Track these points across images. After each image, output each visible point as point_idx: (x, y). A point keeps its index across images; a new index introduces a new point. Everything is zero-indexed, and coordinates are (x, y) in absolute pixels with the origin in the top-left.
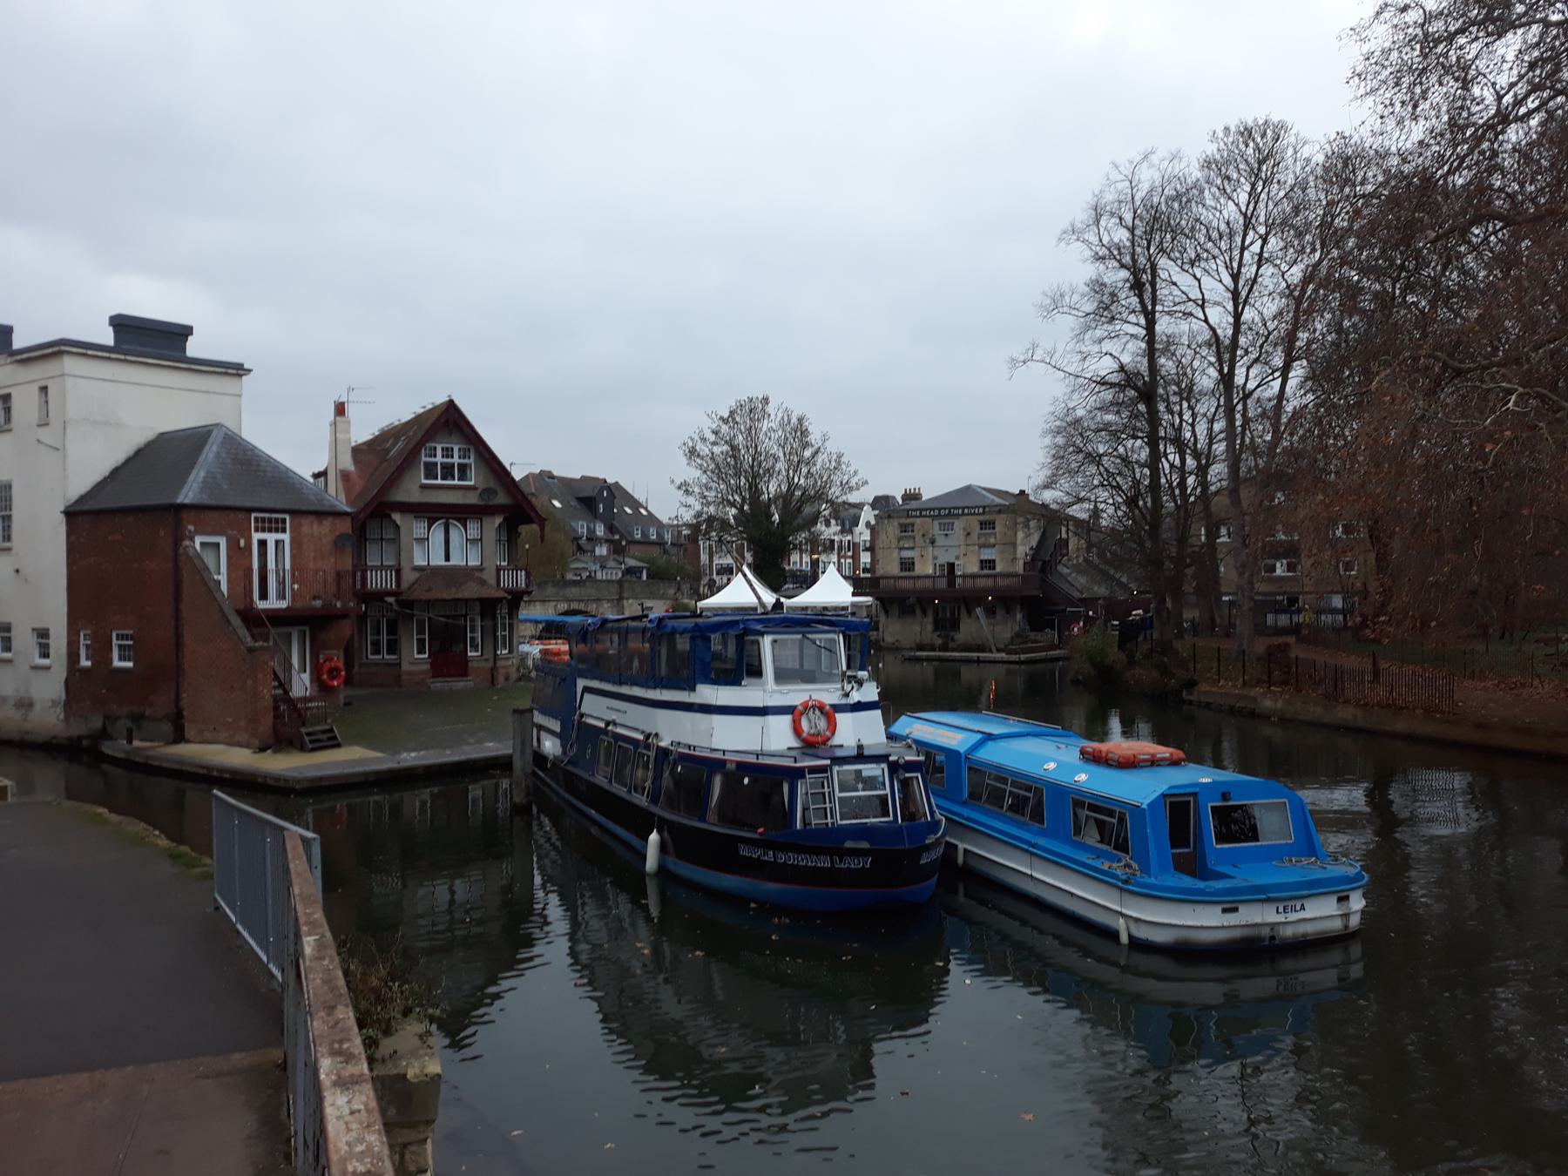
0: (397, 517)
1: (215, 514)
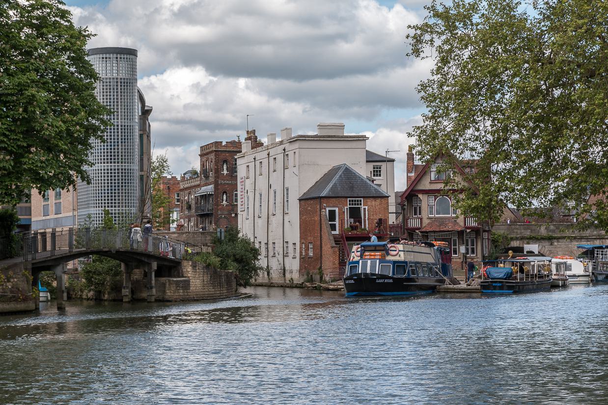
0: (420, 196)
1: (334, 199)
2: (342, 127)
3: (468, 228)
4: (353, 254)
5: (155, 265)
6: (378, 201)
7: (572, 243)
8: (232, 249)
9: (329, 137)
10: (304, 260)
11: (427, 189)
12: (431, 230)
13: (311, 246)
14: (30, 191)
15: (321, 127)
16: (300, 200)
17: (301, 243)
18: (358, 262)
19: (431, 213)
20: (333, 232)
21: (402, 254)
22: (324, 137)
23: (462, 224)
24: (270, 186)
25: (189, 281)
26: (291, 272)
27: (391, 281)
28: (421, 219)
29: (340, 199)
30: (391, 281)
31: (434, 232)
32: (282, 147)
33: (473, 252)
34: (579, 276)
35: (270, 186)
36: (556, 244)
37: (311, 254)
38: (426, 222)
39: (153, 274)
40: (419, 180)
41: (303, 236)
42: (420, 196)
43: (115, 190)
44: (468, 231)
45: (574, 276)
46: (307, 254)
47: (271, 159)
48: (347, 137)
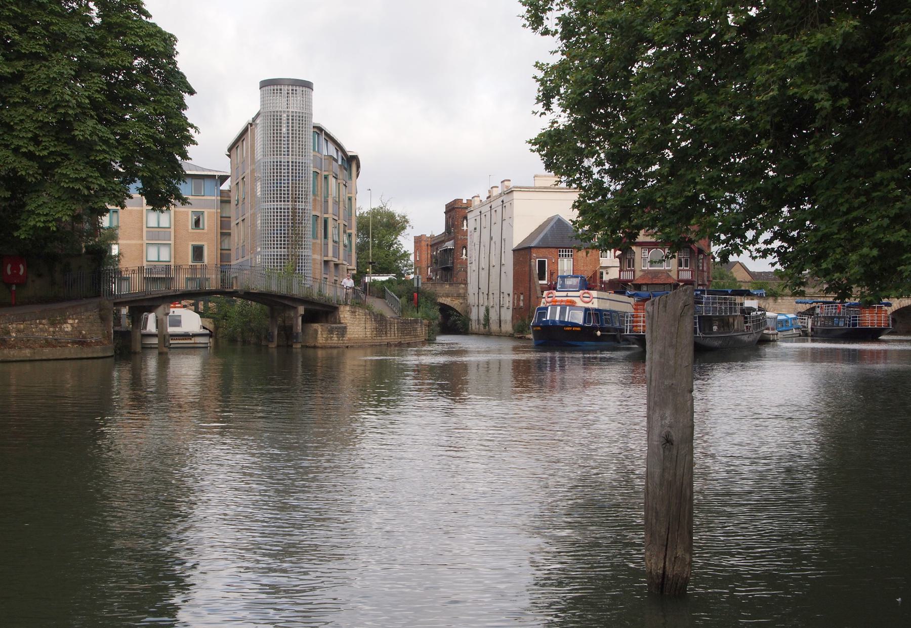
0: (634, 248)
1: (544, 250)
3: (682, 281)
4: (543, 300)
5: (301, 310)
9: (545, 188)
10: (516, 310)
12: (644, 282)
13: (522, 298)
16: (514, 251)
17: (514, 294)
18: (546, 308)
20: (541, 282)
21: (595, 301)
22: (540, 188)
23: (675, 277)
24: (491, 238)
25: (345, 328)
26: (506, 322)
27: (579, 329)
30: (579, 329)
31: (647, 285)
32: (501, 199)
34: (194, 335)
35: (491, 238)
37: (522, 304)
38: (638, 274)
39: (300, 318)
41: (516, 287)
45: (186, 336)
46: (518, 304)
47: (493, 211)
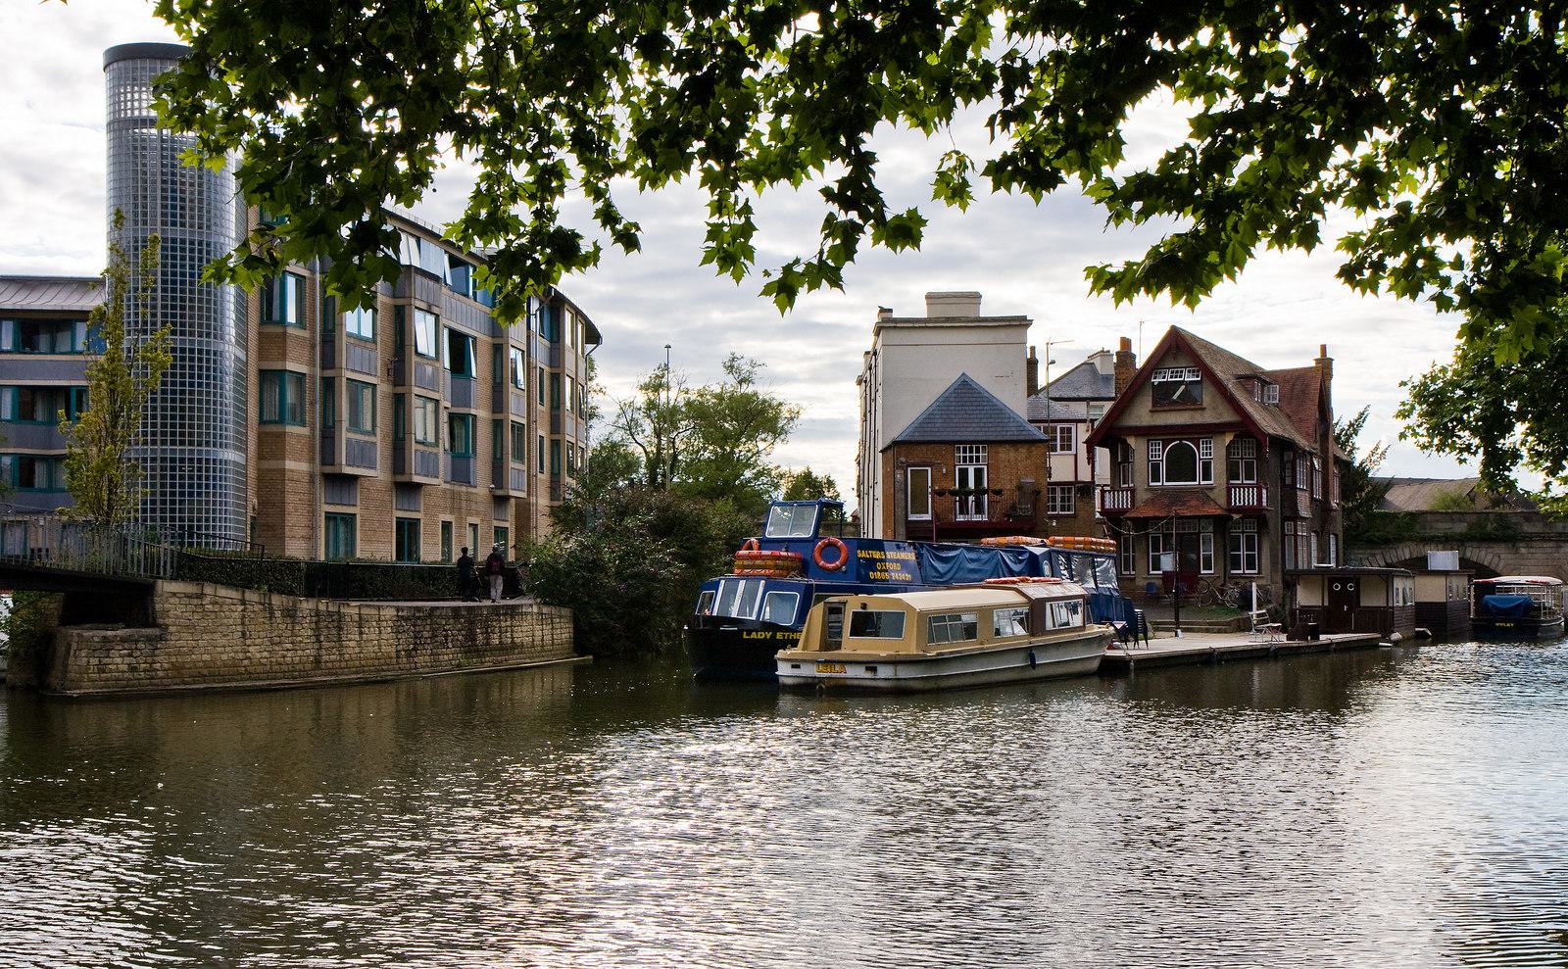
0: (1131, 441)
1: (924, 448)
2: (976, 297)
3: (1238, 510)
6: (1023, 450)
7: (1562, 550)
8: (947, 724)
9: (948, 319)
11: (1145, 424)
14: (944, 28)
15: (932, 298)
19: (1156, 478)
23: (1222, 501)
28: (1133, 491)
29: (937, 447)
33: (1251, 565)
36: (1523, 550)
40: (494, 370)
42: (1131, 441)
43: (173, 426)
44: (1236, 516)
48: (986, 320)
